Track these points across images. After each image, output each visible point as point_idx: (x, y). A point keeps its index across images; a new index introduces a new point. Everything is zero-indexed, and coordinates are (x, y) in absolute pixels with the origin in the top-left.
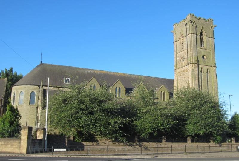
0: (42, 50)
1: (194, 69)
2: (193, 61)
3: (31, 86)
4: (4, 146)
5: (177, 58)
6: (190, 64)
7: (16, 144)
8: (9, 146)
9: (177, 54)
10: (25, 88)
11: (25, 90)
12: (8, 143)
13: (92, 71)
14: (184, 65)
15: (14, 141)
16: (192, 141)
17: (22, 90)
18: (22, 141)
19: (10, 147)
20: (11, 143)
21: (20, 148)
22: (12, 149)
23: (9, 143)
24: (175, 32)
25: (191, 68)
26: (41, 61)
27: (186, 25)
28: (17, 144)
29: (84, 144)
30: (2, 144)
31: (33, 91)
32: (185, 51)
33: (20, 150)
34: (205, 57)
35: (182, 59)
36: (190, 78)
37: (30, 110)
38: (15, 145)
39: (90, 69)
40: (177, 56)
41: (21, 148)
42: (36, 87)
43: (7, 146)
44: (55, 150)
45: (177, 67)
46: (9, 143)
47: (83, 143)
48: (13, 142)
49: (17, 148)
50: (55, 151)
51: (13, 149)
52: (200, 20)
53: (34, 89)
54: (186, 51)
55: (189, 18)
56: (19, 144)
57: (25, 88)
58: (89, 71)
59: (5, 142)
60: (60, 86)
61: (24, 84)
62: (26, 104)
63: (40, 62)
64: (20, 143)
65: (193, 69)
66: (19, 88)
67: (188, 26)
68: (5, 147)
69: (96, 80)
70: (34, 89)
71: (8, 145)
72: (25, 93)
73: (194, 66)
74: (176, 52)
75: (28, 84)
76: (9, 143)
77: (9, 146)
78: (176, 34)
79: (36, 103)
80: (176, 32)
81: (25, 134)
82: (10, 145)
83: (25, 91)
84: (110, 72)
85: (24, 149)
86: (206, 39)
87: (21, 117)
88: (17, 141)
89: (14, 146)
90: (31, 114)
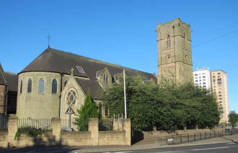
0: (49, 33)
1: (181, 67)
2: (180, 60)
3: (53, 73)
4: (110, 139)
5: (162, 55)
6: (178, 62)
7: (121, 136)
8: (115, 139)
9: (161, 51)
10: (46, 75)
11: (46, 77)
12: (114, 136)
13: (93, 61)
14: (170, 62)
15: (119, 133)
16: (199, 128)
17: (43, 77)
18: (126, 133)
19: (116, 140)
20: (116, 135)
21: (125, 140)
22: (118, 141)
23: (115, 136)
24: (160, 31)
25: (179, 65)
26: (49, 46)
27: (173, 27)
28: (122, 136)
29: (144, 133)
30: (108, 138)
31: (55, 79)
32: (171, 50)
33: (125, 142)
34: (187, 57)
35: (168, 56)
36: (178, 74)
37: (53, 100)
38: (120, 138)
39: (92, 59)
40: (162, 53)
41: (126, 141)
42: (58, 74)
43: (113, 139)
44: (168, 139)
45: (161, 63)
46: (115, 136)
47: (143, 132)
48: (118, 135)
49: (122, 140)
50: (168, 141)
51: (119, 142)
52: (184, 24)
53: (56, 76)
54: (173, 50)
55: (177, 22)
56: (124, 137)
57: (46, 75)
58: (91, 60)
59: (110, 135)
60: (79, 75)
61: (37, 70)
62: (48, 93)
63: (48, 47)
64: (124, 135)
65: (181, 67)
66: (38, 75)
67: (176, 29)
68: (111, 140)
69: (109, 71)
70: (56, 76)
71: (114, 138)
72: (47, 81)
73: (181, 64)
74: (161, 50)
75: (48, 70)
76: (115, 136)
77: (115, 139)
78: (161, 33)
79: (58, 92)
80: (161, 31)
81: (128, 126)
82: (116, 138)
83: (47, 79)
84: (107, 63)
85: (129, 141)
86: (186, 41)
87: (234, 111)
88: (122, 134)
89: (120, 139)
90: (54, 104)
